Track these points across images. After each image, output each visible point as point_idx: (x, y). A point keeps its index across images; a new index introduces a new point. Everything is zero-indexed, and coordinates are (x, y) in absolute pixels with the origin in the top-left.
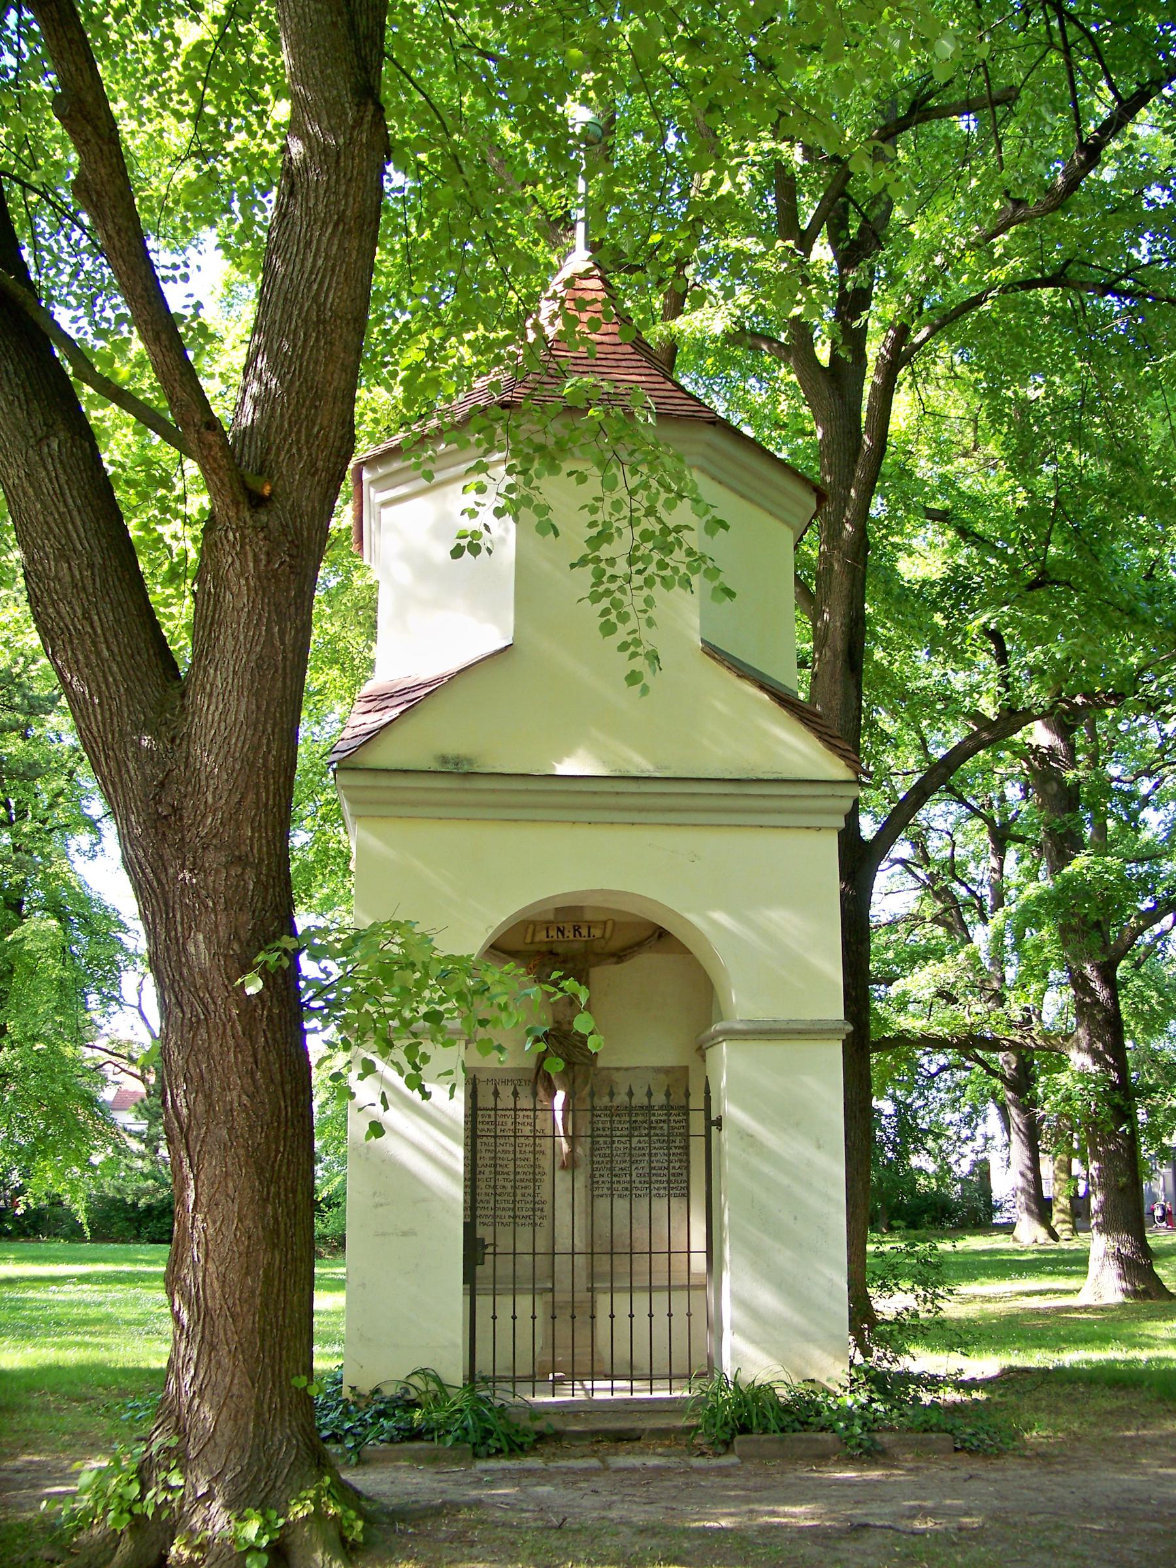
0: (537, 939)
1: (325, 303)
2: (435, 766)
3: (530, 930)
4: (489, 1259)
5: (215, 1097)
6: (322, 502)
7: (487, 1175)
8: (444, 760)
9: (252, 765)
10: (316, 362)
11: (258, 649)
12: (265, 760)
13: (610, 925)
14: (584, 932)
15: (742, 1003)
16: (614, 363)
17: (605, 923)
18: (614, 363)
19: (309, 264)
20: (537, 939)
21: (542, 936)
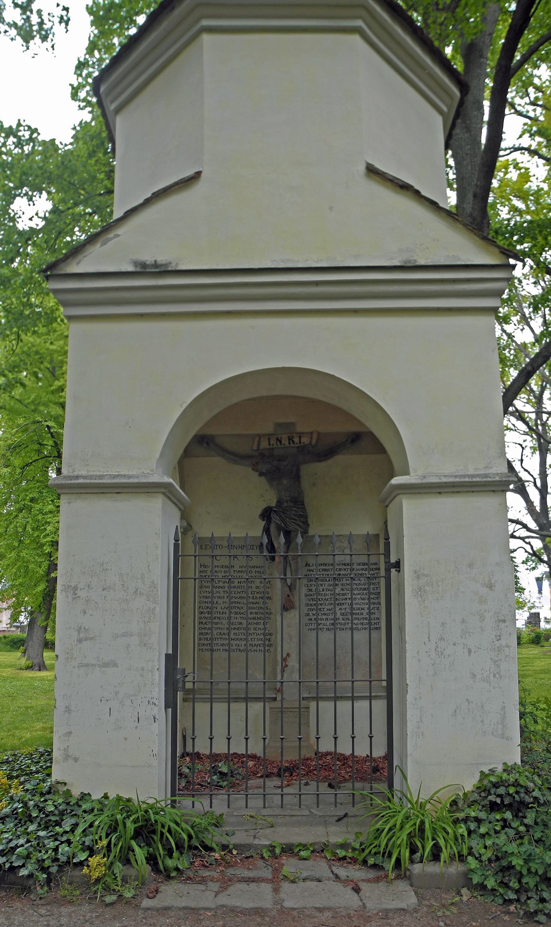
0: (262, 447)
14: (296, 440)
17: (312, 433)
21: (264, 444)
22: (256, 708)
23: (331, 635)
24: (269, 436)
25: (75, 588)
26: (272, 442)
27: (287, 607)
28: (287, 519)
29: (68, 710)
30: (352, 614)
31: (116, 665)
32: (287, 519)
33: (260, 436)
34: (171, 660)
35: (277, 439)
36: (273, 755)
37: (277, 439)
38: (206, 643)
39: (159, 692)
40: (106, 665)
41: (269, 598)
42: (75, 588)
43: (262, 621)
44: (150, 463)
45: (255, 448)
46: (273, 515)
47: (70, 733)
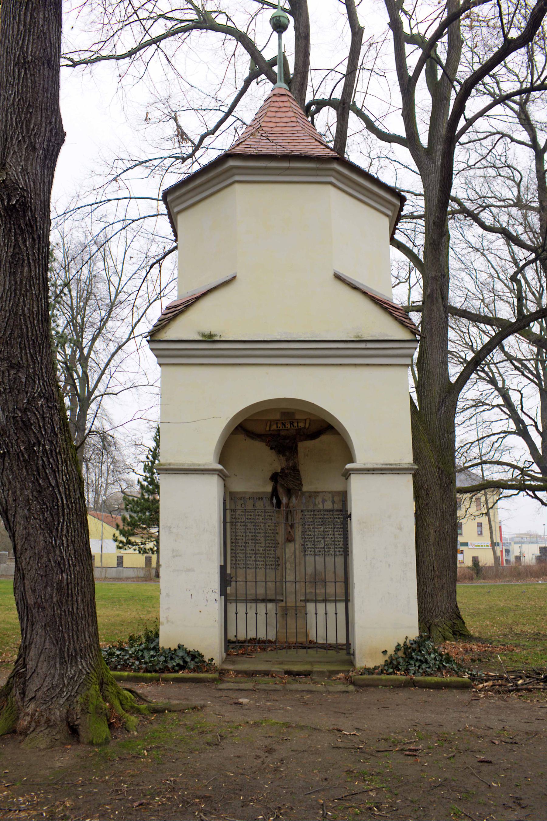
0: (272, 429)
1: (27, 52)
2: (199, 338)
3: (268, 424)
4: (233, 584)
5: (18, 493)
6: (43, 166)
7: (250, 544)
8: (204, 335)
9: (16, 314)
10: (27, 86)
11: (11, 250)
12: (23, 311)
13: (308, 422)
14: (295, 424)
15: (363, 457)
16: (284, 125)
17: (306, 420)
18: (284, 125)
19: (16, 31)
20: (272, 429)
21: (274, 427)
22: (270, 606)
23: (312, 558)
24: (277, 422)
25: (170, 527)
26: (279, 425)
27: (290, 539)
28: (286, 482)
29: (168, 595)
30: (334, 545)
31: (193, 571)
32: (286, 482)
33: (271, 421)
34: (223, 569)
35: (282, 423)
36: (282, 638)
37: (282, 423)
38: (235, 565)
39: (216, 585)
40: (188, 570)
41: (277, 533)
42: (170, 527)
43: (273, 549)
44: (208, 457)
45: (268, 428)
46: (279, 479)
47: (169, 608)
